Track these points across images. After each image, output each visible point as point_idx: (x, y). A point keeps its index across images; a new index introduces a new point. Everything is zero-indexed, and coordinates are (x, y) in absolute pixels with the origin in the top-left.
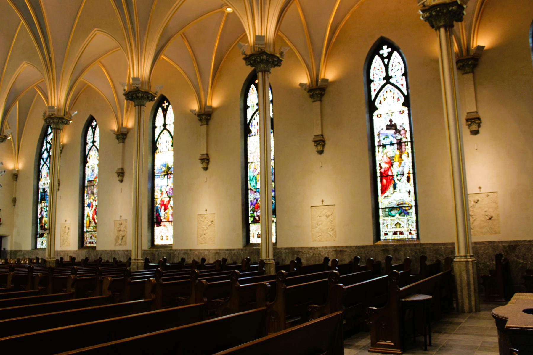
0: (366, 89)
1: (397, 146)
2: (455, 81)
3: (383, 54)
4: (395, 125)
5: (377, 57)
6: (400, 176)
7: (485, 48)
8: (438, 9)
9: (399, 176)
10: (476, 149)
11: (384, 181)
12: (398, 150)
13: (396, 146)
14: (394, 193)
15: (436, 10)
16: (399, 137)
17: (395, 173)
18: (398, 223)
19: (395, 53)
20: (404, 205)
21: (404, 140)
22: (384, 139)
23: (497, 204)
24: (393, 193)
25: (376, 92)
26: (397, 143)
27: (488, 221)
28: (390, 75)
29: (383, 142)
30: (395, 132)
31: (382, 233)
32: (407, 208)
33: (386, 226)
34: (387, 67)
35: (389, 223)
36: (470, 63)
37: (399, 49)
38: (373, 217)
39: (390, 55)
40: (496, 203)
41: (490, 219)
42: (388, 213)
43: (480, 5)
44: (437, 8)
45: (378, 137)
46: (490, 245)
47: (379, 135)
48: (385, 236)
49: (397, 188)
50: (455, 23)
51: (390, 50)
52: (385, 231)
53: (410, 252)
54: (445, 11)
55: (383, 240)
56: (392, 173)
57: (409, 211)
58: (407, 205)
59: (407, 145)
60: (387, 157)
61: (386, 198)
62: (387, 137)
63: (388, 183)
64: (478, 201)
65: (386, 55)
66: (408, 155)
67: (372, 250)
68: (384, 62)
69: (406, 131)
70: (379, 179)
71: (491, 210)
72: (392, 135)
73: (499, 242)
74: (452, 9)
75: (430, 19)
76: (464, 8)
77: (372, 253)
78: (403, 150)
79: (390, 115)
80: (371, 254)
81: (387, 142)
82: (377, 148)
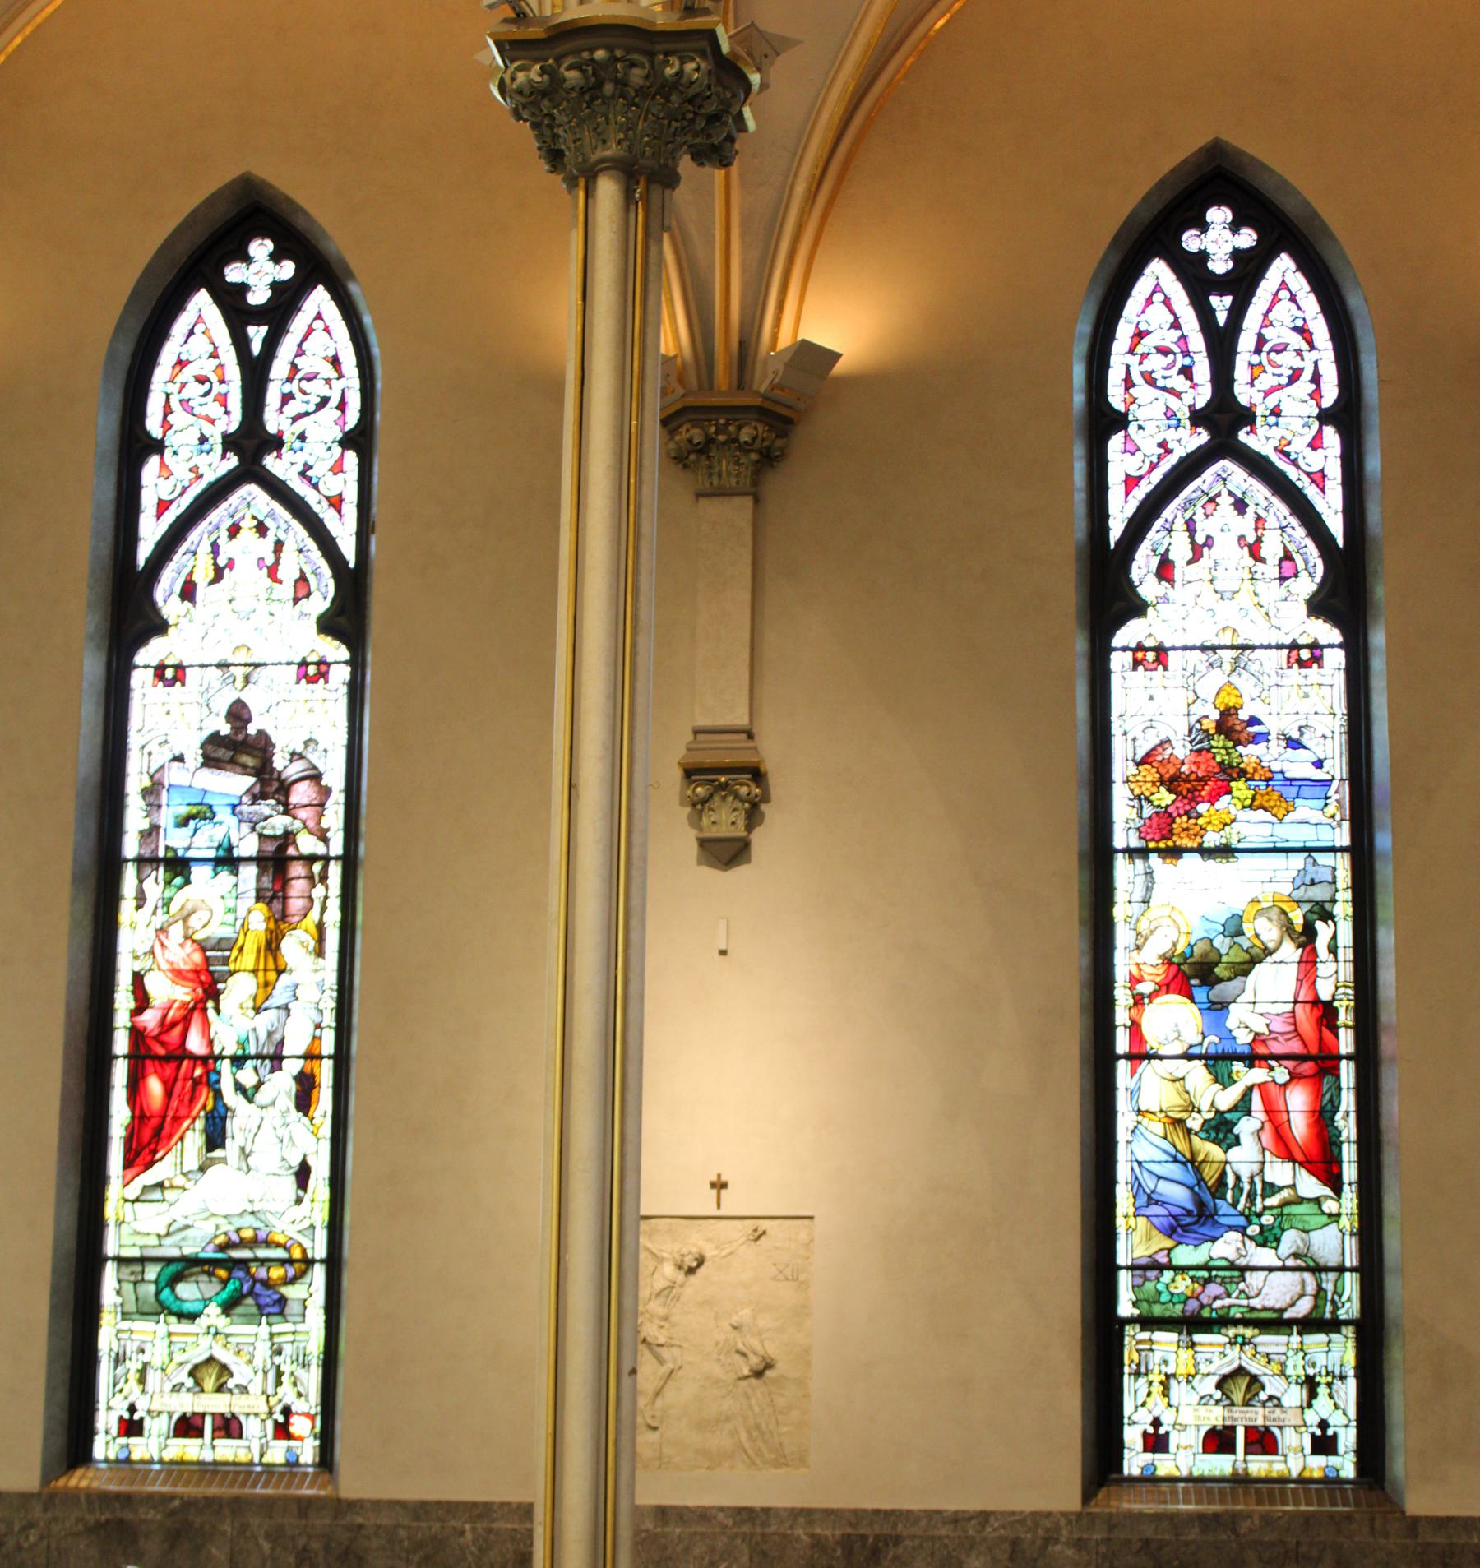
0: (106, 490)
1: (259, 878)
2: (644, 513)
3: (243, 288)
4: (262, 747)
5: (202, 303)
6: (256, 1069)
7: (839, 368)
8: (600, 54)
9: (249, 1064)
10: (723, 953)
11: (155, 1086)
12: (261, 905)
13: (249, 872)
14: (211, 1171)
15: (585, 55)
16: (279, 823)
17: (226, 1042)
18: (211, 1360)
19: (319, 299)
20: (262, 1253)
21: (307, 844)
22: (184, 822)
23: (803, 1286)
24: (202, 1169)
25: (170, 516)
26: (260, 860)
27: (744, 1383)
28: (272, 428)
29: (175, 839)
30: (257, 789)
31: (106, 1419)
32: (276, 1273)
33: (133, 1377)
34: (255, 374)
35: (157, 1355)
36: (745, 435)
37: (350, 275)
38: (54, 1309)
39: (286, 300)
40: (797, 1280)
41: (758, 1374)
42: (158, 1293)
43: (839, 111)
44: (592, 50)
45: (142, 804)
46: (746, 1528)
47: (152, 792)
48: (123, 1440)
49: (228, 1141)
50: (686, 165)
51: (287, 270)
52: (126, 1405)
53: (266, 1546)
54: (637, 76)
55: (107, 1460)
56: (211, 1043)
57: (289, 1291)
58: (280, 1253)
59: (324, 878)
60: (187, 937)
61: (157, 1195)
62: (201, 813)
63: (174, 1103)
64: (701, 1261)
65: (259, 296)
66: (321, 940)
67: (31, 1525)
68: (240, 342)
69: (326, 792)
70: (120, 1073)
71: (764, 1321)
72: (234, 807)
73: (796, 1514)
74: (680, 74)
75: (545, 104)
76: (747, 86)
77: (26, 1545)
78: (296, 904)
79: (240, 683)
80: (19, 1548)
81: (203, 842)
82: (130, 874)
